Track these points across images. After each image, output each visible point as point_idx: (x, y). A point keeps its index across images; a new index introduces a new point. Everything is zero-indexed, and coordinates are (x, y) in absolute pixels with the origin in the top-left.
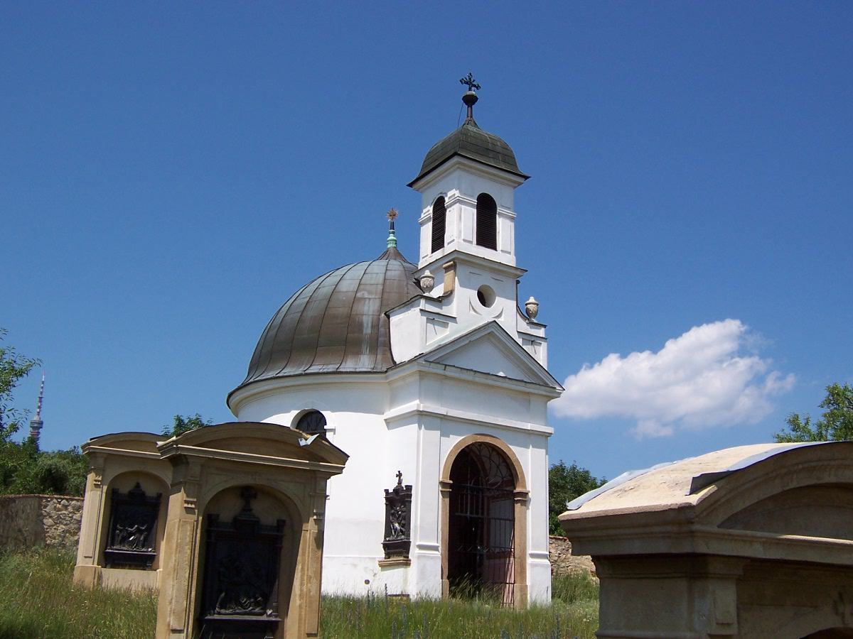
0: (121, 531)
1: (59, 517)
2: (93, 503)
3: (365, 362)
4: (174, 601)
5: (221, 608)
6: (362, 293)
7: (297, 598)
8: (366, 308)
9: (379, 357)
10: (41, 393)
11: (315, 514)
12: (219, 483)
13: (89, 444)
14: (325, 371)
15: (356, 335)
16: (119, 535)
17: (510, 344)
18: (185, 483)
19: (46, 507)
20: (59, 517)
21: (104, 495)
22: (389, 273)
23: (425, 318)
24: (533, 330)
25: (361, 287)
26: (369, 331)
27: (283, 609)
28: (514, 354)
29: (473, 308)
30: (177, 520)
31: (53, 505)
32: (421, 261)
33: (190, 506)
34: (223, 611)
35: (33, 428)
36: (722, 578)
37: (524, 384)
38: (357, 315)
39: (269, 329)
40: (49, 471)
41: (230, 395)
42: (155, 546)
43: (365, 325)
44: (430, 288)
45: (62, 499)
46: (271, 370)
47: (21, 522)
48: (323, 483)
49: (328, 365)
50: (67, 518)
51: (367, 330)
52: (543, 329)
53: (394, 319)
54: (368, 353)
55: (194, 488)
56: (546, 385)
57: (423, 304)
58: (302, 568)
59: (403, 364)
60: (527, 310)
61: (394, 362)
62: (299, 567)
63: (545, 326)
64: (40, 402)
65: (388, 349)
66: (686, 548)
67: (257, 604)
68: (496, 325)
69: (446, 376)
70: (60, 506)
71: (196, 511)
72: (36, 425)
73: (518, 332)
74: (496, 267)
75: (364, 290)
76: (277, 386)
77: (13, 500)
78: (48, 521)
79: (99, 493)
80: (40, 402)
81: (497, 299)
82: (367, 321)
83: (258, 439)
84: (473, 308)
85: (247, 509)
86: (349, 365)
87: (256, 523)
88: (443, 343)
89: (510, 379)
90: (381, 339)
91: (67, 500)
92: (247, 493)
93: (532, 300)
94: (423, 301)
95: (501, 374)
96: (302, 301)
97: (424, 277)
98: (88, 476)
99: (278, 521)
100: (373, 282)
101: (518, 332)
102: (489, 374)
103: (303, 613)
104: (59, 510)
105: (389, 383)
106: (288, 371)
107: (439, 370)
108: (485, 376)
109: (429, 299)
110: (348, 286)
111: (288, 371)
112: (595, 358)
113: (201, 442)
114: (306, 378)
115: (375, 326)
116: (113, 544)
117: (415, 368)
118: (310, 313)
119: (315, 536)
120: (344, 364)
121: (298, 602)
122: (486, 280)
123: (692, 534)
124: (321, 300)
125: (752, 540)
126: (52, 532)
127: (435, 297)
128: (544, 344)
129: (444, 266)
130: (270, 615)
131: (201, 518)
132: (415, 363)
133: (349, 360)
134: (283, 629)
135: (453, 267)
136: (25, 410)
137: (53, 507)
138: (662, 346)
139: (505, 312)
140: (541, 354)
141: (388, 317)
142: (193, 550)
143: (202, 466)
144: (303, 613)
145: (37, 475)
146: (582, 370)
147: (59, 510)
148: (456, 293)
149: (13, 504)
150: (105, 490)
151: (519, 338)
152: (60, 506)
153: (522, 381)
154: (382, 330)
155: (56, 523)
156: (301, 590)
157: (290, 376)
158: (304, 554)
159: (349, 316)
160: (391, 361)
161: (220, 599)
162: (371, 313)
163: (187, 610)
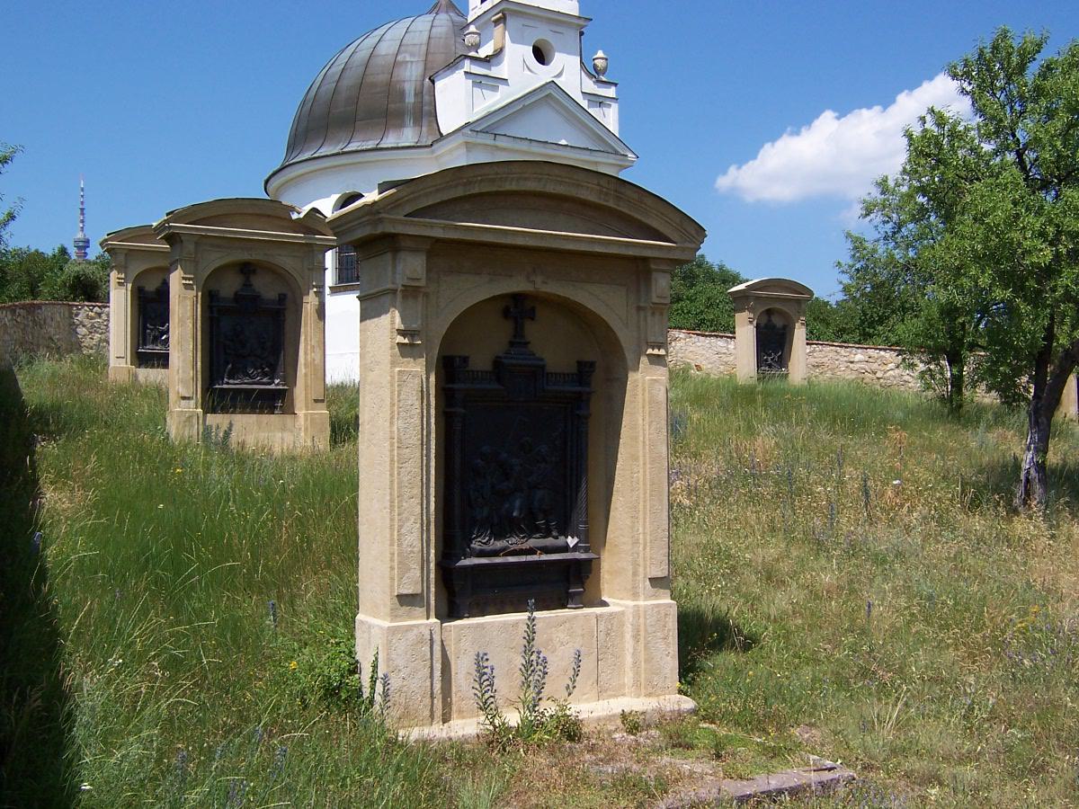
0: (152, 330)
1: (93, 326)
2: (119, 301)
3: (408, 136)
4: (180, 371)
5: (229, 379)
6: (403, 55)
7: (303, 367)
8: (408, 74)
9: (424, 129)
10: (82, 203)
11: (314, 286)
12: (215, 260)
13: (106, 240)
14: (364, 148)
15: (398, 105)
16: (150, 335)
17: (580, 114)
18: (181, 260)
19: (77, 315)
20: (93, 326)
21: (129, 293)
22: (434, 30)
23: (471, 81)
24: (600, 89)
25: (402, 48)
26: (412, 100)
27: (291, 379)
28: (579, 121)
29: (529, 69)
30: (177, 297)
31: (84, 312)
32: (471, 13)
33: (187, 282)
34: (231, 381)
35: (79, 247)
36: (415, 251)
37: (588, 152)
38: (398, 81)
39: (304, 103)
40: (77, 277)
41: (267, 182)
42: (587, 532)
43: (407, 92)
44: (476, 47)
45: (94, 307)
46: (306, 151)
47: (52, 331)
48: (320, 256)
49: (367, 141)
50: (102, 327)
51: (410, 99)
52: (613, 88)
53: (439, 85)
54: (412, 124)
55: (192, 265)
56: (616, 153)
57: (467, 66)
58: (306, 339)
59: (449, 135)
60: (595, 67)
61: (441, 134)
62: (302, 338)
63: (616, 85)
64: (83, 214)
65: (434, 118)
66: (379, 230)
67: (265, 375)
68: (554, 86)
69: (496, 147)
70: (93, 314)
71: (195, 287)
72: (81, 244)
73: (582, 93)
74: (550, 15)
75: (406, 52)
76: (336, 163)
77: (39, 306)
78: (83, 331)
79: (124, 291)
80: (83, 214)
81: (557, 54)
82: (410, 89)
83: (250, 214)
84: (529, 69)
85: (247, 285)
86: (390, 140)
87: (256, 298)
88: (493, 109)
89: (572, 147)
90: (426, 108)
91: (99, 307)
92: (246, 269)
93: (600, 54)
94: (467, 62)
95: (563, 142)
96: (337, 68)
97: (469, 33)
98: (111, 275)
99: (279, 295)
100: (415, 42)
101: (582, 93)
102: (546, 142)
103: (309, 382)
104: (92, 318)
105: (436, 158)
106: (323, 152)
107: (488, 140)
108: (542, 145)
109: (475, 60)
110: (387, 48)
111: (324, 151)
112: (801, 120)
113: (192, 220)
114: (343, 157)
115: (419, 93)
116: (145, 344)
117: (460, 139)
118: (346, 83)
119: (317, 307)
120: (384, 139)
121: (304, 371)
122: (542, 33)
123: (381, 220)
124: (357, 66)
125: (432, 226)
126: (87, 342)
127: (483, 56)
128: (615, 106)
129: (494, 18)
130: (278, 384)
131: (200, 294)
132: (460, 134)
133: (391, 132)
134: (293, 400)
135: (503, 20)
136: (19, 198)
137: (85, 315)
138: (893, 101)
139: (566, 70)
140: (610, 118)
141: (433, 82)
142: (195, 324)
143: (196, 243)
144: (309, 382)
145: (64, 283)
146: (785, 136)
147: (92, 318)
148: (507, 50)
149: (39, 311)
150: (129, 288)
151: (584, 99)
152: (93, 314)
153: (587, 149)
154: (426, 98)
155: (91, 333)
156: (306, 359)
157: (327, 156)
158: (306, 324)
159: (389, 84)
160: (437, 133)
161: (227, 370)
162: (414, 78)
163: (195, 379)
